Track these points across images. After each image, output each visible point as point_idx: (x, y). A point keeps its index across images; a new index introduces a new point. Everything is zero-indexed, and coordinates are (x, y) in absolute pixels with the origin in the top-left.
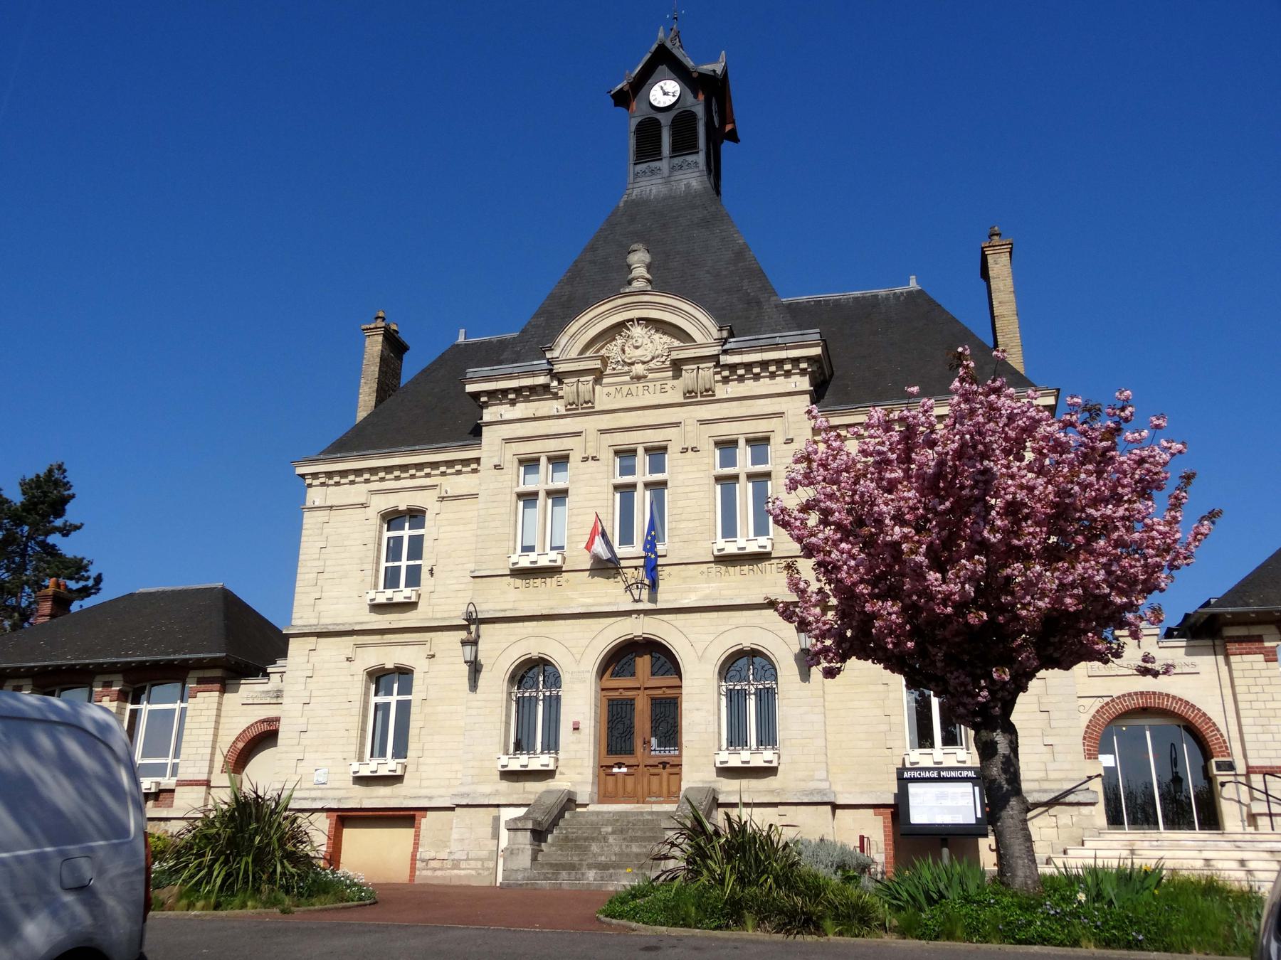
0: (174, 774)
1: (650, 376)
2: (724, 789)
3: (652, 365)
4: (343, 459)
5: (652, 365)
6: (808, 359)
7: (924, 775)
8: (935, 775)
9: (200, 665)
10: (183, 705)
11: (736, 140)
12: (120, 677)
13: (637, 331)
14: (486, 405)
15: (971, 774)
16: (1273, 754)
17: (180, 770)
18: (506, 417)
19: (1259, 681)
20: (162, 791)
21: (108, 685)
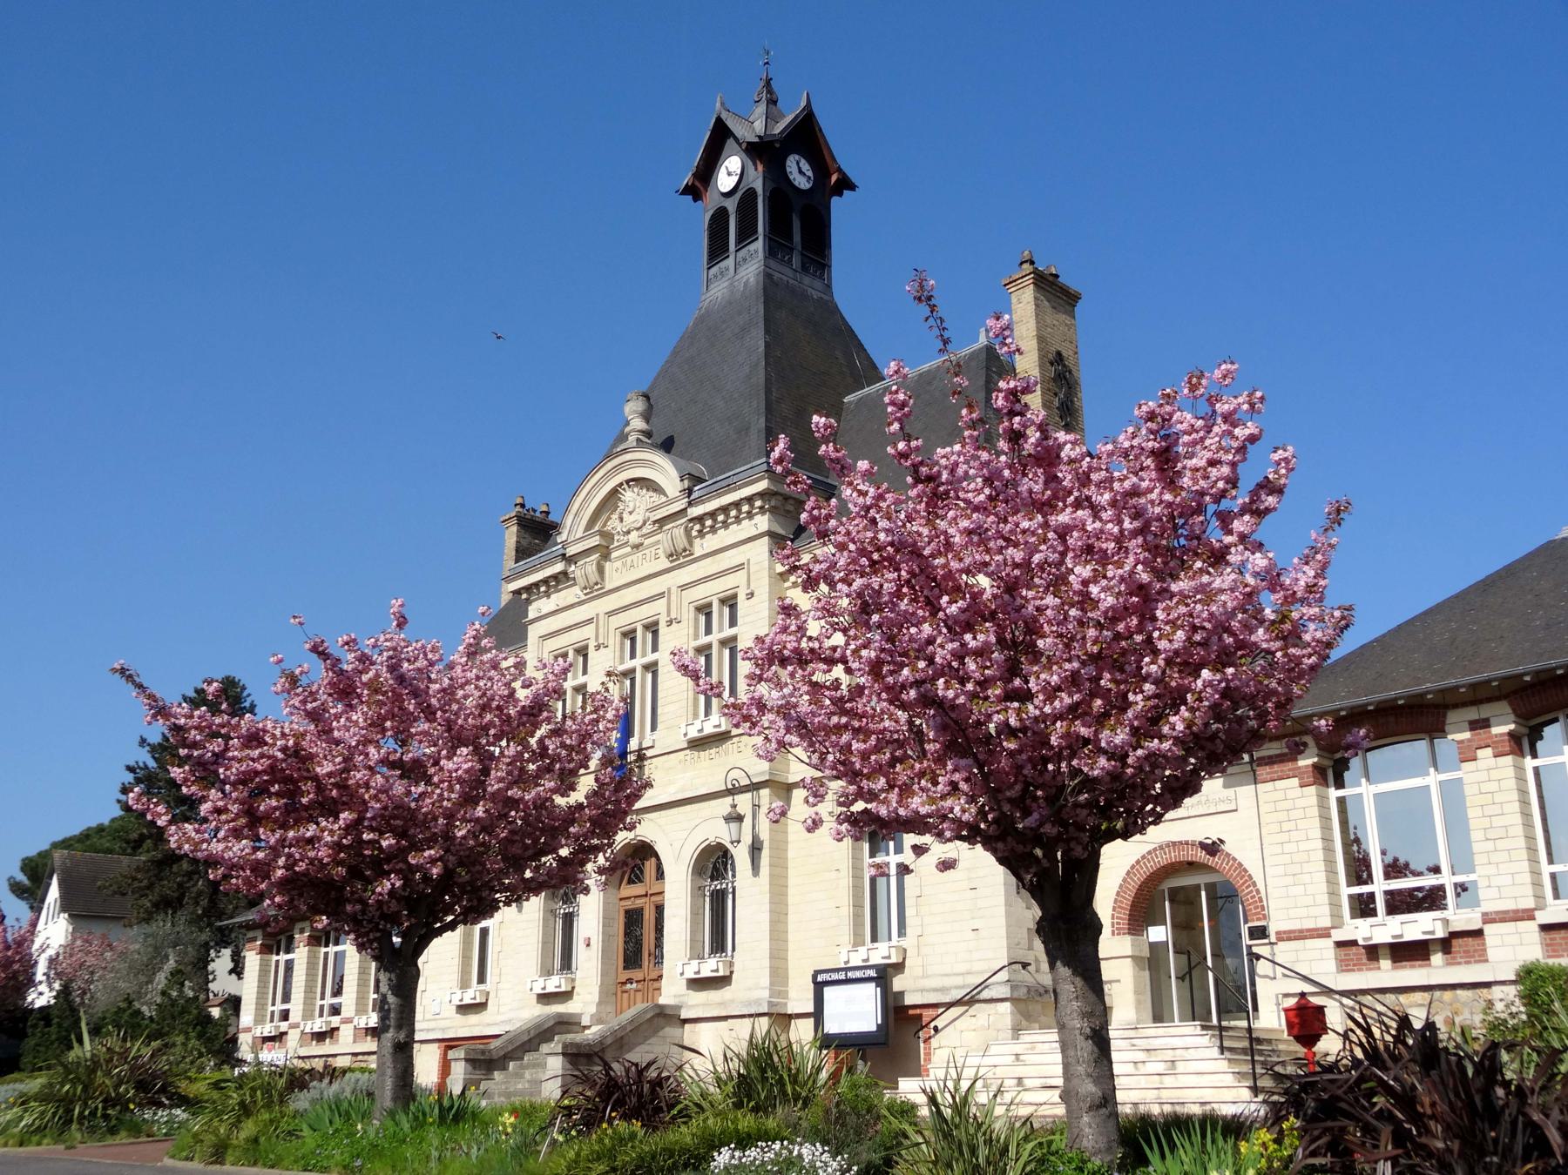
1: (647, 542)
5: (644, 531)
6: (761, 495)
7: (835, 977)
8: (842, 976)
11: (852, 187)
12: (1503, 707)
13: (628, 495)
14: (528, 602)
15: (872, 973)
16: (1303, 912)
18: (544, 611)
19: (1294, 815)
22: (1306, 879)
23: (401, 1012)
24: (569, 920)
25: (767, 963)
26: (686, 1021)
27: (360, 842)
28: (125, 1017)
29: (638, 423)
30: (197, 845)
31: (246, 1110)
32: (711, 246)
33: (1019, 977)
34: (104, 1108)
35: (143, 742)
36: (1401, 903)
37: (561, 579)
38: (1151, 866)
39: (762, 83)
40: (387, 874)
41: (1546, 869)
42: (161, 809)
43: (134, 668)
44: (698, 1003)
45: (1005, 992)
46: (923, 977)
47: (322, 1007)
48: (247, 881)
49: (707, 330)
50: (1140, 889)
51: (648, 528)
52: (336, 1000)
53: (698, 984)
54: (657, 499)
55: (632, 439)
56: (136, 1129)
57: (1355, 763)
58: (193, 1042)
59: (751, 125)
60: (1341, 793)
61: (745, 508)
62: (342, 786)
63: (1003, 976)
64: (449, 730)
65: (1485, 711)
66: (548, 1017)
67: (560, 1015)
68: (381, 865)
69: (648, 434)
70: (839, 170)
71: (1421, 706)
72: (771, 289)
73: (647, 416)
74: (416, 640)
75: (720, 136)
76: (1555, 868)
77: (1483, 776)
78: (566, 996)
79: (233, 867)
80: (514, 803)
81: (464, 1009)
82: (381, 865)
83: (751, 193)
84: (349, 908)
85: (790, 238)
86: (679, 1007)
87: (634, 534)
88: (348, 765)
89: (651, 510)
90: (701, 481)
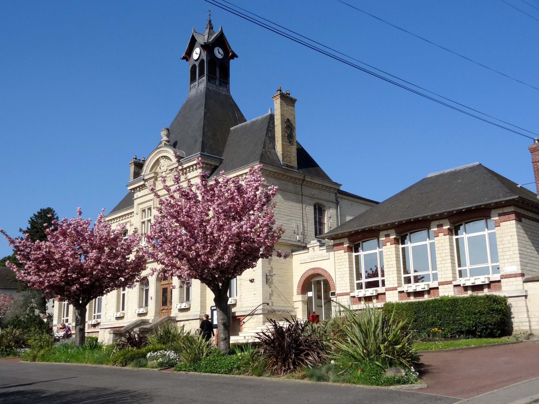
0: (383, 285)
2: (179, 316)
3: (167, 172)
4: (121, 212)
5: (167, 172)
9: (498, 205)
10: (380, 250)
11: (237, 57)
12: (447, 221)
14: (134, 193)
16: (343, 288)
17: (439, 276)
18: (139, 196)
20: (379, 294)
21: (387, 236)
22: (345, 279)
23: (81, 320)
24: (147, 291)
25: (200, 304)
26: (178, 321)
27: (67, 276)
28: (16, 322)
29: (165, 138)
30: (23, 278)
31: (41, 347)
32: (191, 77)
33: (266, 308)
34: (6, 349)
35: (21, 230)
36: (369, 285)
37: (143, 187)
38: (307, 275)
39: (208, 22)
40: (75, 284)
41: (458, 269)
42: (15, 266)
43: (5, 230)
44: (181, 316)
45: (261, 312)
46: (241, 307)
47: (94, 316)
48: (38, 286)
49: (188, 106)
50: (305, 281)
51: (168, 172)
52: (99, 314)
53: (181, 310)
54: (170, 162)
55: (163, 143)
56: (15, 354)
57: (462, 228)
58: (37, 330)
59: (202, 39)
60: (457, 237)
61: (195, 167)
62: (62, 261)
63: (261, 307)
64: (91, 245)
65: (441, 222)
66: (139, 321)
67: (143, 320)
68: (73, 281)
69: (168, 141)
70: (232, 51)
71: (425, 220)
72: (208, 94)
73: (168, 136)
74: (85, 218)
75: (193, 42)
76: (460, 269)
77: (387, 250)
78: (145, 314)
79: (34, 283)
80: (109, 264)
81: (118, 318)
82: (73, 281)
83: (203, 61)
84: (65, 293)
85: (215, 75)
86: (176, 317)
87: (164, 173)
88: (63, 255)
89: (168, 166)
90: (183, 158)
